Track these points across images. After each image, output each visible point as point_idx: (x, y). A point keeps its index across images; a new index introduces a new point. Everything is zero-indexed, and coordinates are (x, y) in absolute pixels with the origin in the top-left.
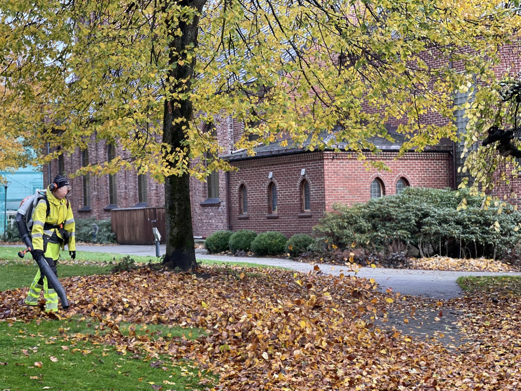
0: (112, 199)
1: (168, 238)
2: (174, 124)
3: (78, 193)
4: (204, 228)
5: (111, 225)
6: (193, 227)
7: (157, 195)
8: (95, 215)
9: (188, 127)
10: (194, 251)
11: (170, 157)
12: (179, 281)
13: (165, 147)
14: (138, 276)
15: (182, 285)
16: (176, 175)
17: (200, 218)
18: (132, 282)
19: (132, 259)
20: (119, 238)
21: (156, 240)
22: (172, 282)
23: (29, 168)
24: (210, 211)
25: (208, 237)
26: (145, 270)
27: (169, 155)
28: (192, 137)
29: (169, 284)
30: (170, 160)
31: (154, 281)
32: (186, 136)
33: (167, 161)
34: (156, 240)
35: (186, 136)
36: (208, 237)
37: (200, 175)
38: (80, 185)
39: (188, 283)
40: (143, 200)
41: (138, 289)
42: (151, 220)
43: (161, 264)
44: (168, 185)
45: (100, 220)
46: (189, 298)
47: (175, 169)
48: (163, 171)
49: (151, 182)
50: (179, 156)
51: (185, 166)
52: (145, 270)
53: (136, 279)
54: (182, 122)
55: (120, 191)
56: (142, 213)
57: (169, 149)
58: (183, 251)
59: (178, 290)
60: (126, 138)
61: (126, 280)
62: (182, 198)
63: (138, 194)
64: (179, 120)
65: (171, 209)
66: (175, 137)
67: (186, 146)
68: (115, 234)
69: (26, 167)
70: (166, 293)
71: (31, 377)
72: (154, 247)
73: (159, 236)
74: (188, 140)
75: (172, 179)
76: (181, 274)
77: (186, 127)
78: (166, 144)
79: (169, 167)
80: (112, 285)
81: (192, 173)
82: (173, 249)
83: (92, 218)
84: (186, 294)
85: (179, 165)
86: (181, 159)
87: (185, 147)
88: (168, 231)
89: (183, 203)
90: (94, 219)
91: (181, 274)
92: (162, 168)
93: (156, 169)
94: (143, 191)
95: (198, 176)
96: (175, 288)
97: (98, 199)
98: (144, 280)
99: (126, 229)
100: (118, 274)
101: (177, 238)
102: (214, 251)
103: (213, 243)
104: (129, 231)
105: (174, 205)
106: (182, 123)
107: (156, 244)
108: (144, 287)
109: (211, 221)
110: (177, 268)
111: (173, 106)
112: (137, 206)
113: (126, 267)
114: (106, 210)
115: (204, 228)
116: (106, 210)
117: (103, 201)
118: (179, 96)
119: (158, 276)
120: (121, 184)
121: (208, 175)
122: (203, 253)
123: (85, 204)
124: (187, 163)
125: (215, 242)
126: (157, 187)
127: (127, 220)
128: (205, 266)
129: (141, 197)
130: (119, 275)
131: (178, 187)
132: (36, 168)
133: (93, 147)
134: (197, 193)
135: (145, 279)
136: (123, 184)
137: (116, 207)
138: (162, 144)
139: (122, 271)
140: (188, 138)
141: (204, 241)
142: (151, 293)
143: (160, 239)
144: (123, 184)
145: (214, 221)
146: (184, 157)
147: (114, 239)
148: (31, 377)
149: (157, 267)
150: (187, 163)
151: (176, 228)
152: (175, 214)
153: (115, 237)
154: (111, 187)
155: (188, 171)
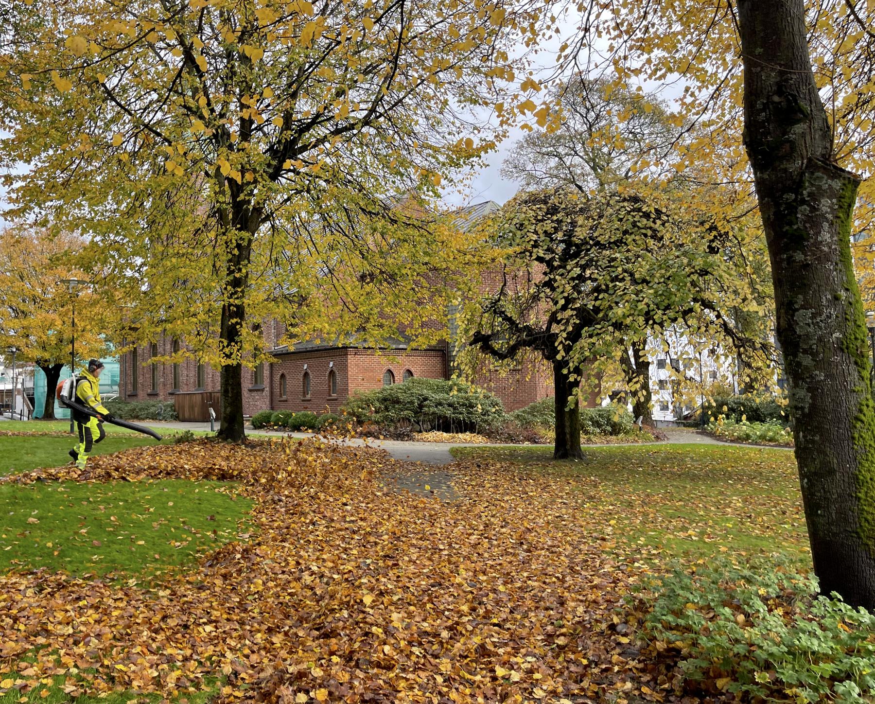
0: (176, 385)
1: (223, 415)
9: (242, 326)
11: (227, 350)
15: (234, 454)
18: (192, 451)
20: (181, 416)
25: (254, 416)
29: (222, 453)
36: (254, 416)
37: (250, 365)
45: (164, 401)
55: (182, 379)
60: (189, 335)
64: (234, 321)
65: (225, 392)
66: (231, 334)
72: (210, 424)
75: (227, 368)
81: (244, 363)
82: (226, 425)
93: (214, 359)
95: (248, 366)
97: (164, 385)
99: (187, 409)
106: (237, 323)
110: (229, 440)
122: (249, 429)
123: (153, 389)
129: (200, 383)
131: (232, 374)
136: (185, 372)
144: (185, 372)
146: (238, 351)
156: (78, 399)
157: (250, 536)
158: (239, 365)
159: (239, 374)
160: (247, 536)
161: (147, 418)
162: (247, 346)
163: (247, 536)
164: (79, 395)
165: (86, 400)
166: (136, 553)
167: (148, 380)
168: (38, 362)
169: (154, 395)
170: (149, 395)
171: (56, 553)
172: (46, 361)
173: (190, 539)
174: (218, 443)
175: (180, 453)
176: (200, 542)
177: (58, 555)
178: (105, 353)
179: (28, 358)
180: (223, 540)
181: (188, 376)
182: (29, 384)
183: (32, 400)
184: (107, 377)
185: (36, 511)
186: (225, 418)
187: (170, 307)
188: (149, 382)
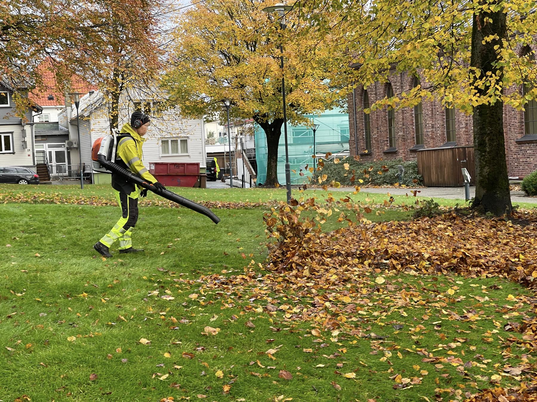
0: (419, 139)
1: (478, 178)
2: (484, 43)
3: (384, 134)
4: (521, 168)
5: (417, 166)
6: (508, 166)
7: (467, 133)
8: (400, 157)
9: (502, 46)
10: (509, 193)
11: (480, 84)
12: (491, 229)
13: (473, 72)
14: (442, 222)
15: (495, 234)
16: (487, 104)
17: (515, 156)
18: (435, 230)
19: (436, 203)
20: (426, 180)
21: (466, 181)
22: (482, 230)
23: (336, 110)
24: (528, 148)
25: (525, 178)
26: (449, 215)
27: (478, 80)
28: (506, 57)
29: (479, 233)
30: (479, 87)
31: (461, 228)
32: (498, 57)
33: (476, 88)
34: (466, 181)
35: (498, 57)
36: (525, 178)
37: (516, 103)
38: (385, 125)
39: (501, 231)
40: (452, 139)
41: (441, 238)
42: (460, 160)
43: (470, 208)
44: (478, 117)
45: (405, 160)
46: (503, 250)
47: (485, 97)
48: (471, 100)
49: (460, 120)
50: (490, 82)
51: (498, 93)
52: (449, 215)
53: (439, 226)
54: (494, 40)
55: (427, 130)
56: (451, 153)
57: (478, 74)
58: (495, 193)
59: (490, 240)
60: (430, 69)
61: (427, 227)
62: (494, 132)
63: (445, 133)
64: (490, 38)
65: (481, 145)
66: (485, 60)
67: (499, 69)
68: (422, 176)
69: (332, 109)
70: (475, 244)
71: (304, 350)
72: (464, 189)
73: (469, 177)
74: (502, 61)
75: (481, 110)
76: (493, 220)
77: (499, 46)
78: (474, 68)
79: (478, 95)
80: (411, 233)
81: (506, 100)
82: (483, 192)
83: (398, 160)
84: (499, 245)
85: (490, 91)
86: (493, 84)
87: (497, 69)
88: (478, 171)
89: (495, 138)
90: (400, 161)
91: (493, 220)
92: (469, 96)
93: (464, 97)
94: (451, 129)
95: (514, 103)
96: (486, 238)
97: (404, 140)
98: (449, 228)
99: (433, 170)
100: (419, 220)
101: (488, 179)
102: (533, 192)
103: (532, 185)
104: (437, 173)
105: (485, 141)
106: (494, 42)
107: (465, 186)
108: (448, 235)
109: (528, 159)
110: (489, 213)
111: (482, 21)
112: (444, 145)
113: (429, 212)
114: (413, 151)
115: (521, 168)
116: (413, 151)
117: (409, 141)
118: (490, 8)
119: (465, 223)
120: (428, 122)
121: (527, 102)
122: (520, 196)
123: (391, 146)
124: (500, 89)
125: (534, 183)
126: (467, 124)
127: (434, 160)
128: (522, 210)
129: (449, 135)
130: (420, 222)
131: (489, 119)
132: (342, 110)
133: (398, 84)
134: (512, 129)
135: (450, 226)
136: (430, 122)
137: (423, 147)
138: (470, 68)
139: (425, 216)
140: (501, 58)
141: (521, 181)
142: (457, 244)
143: (469, 180)
144: (430, 122)
145: (532, 159)
146: (497, 82)
147: (421, 181)
148: (304, 350)
149: (465, 212)
150: (500, 89)
151: (487, 168)
152: (485, 151)
153: (421, 179)
154: (417, 126)
155: (502, 98)
156: (119, 162)
157: (523, 373)
158: (499, 105)
159: (500, 119)
160: (517, 371)
161: (384, 183)
162: (510, 75)
163: (517, 371)
164: (121, 154)
165: (130, 163)
166: (341, 393)
167: (384, 134)
168: (256, 117)
169: (392, 153)
170: (386, 153)
171: (226, 388)
172: (264, 116)
173: (425, 373)
174: (473, 217)
175: (417, 232)
176: (442, 379)
177: (229, 393)
178: (517, 153)
179: (244, 112)
180: (479, 377)
181: (434, 126)
182: (250, 145)
183: (254, 163)
184: (335, 133)
185: (216, 317)
186: (481, 182)
187: (400, 30)
188: (385, 136)
